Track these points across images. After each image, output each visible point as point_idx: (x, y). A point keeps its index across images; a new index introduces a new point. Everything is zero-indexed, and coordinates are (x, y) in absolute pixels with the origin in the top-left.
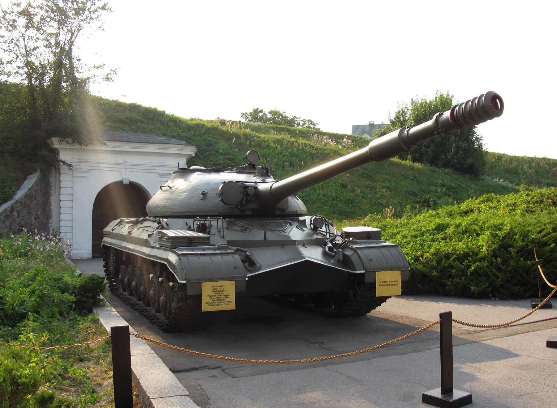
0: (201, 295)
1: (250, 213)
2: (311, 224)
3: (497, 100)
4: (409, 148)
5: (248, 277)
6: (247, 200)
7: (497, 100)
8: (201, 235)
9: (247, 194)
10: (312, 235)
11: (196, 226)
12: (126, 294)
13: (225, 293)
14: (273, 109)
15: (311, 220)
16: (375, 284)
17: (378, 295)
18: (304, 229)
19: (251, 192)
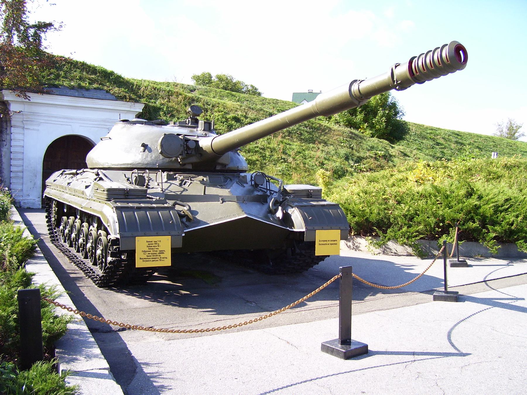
0: (134, 251)
1: (190, 167)
2: (251, 180)
3: (461, 52)
4: (359, 102)
5: (185, 233)
6: (188, 153)
7: (461, 52)
8: (138, 187)
9: (188, 148)
10: (252, 192)
11: (134, 179)
12: (67, 245)
13: (161, 249)
14: (220, 74)
15: (252, 177)
16: (314, 243)
17: (317, 253)
18: (245, 185)
19: (192, 145)
